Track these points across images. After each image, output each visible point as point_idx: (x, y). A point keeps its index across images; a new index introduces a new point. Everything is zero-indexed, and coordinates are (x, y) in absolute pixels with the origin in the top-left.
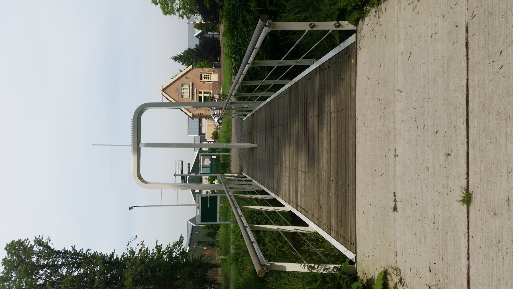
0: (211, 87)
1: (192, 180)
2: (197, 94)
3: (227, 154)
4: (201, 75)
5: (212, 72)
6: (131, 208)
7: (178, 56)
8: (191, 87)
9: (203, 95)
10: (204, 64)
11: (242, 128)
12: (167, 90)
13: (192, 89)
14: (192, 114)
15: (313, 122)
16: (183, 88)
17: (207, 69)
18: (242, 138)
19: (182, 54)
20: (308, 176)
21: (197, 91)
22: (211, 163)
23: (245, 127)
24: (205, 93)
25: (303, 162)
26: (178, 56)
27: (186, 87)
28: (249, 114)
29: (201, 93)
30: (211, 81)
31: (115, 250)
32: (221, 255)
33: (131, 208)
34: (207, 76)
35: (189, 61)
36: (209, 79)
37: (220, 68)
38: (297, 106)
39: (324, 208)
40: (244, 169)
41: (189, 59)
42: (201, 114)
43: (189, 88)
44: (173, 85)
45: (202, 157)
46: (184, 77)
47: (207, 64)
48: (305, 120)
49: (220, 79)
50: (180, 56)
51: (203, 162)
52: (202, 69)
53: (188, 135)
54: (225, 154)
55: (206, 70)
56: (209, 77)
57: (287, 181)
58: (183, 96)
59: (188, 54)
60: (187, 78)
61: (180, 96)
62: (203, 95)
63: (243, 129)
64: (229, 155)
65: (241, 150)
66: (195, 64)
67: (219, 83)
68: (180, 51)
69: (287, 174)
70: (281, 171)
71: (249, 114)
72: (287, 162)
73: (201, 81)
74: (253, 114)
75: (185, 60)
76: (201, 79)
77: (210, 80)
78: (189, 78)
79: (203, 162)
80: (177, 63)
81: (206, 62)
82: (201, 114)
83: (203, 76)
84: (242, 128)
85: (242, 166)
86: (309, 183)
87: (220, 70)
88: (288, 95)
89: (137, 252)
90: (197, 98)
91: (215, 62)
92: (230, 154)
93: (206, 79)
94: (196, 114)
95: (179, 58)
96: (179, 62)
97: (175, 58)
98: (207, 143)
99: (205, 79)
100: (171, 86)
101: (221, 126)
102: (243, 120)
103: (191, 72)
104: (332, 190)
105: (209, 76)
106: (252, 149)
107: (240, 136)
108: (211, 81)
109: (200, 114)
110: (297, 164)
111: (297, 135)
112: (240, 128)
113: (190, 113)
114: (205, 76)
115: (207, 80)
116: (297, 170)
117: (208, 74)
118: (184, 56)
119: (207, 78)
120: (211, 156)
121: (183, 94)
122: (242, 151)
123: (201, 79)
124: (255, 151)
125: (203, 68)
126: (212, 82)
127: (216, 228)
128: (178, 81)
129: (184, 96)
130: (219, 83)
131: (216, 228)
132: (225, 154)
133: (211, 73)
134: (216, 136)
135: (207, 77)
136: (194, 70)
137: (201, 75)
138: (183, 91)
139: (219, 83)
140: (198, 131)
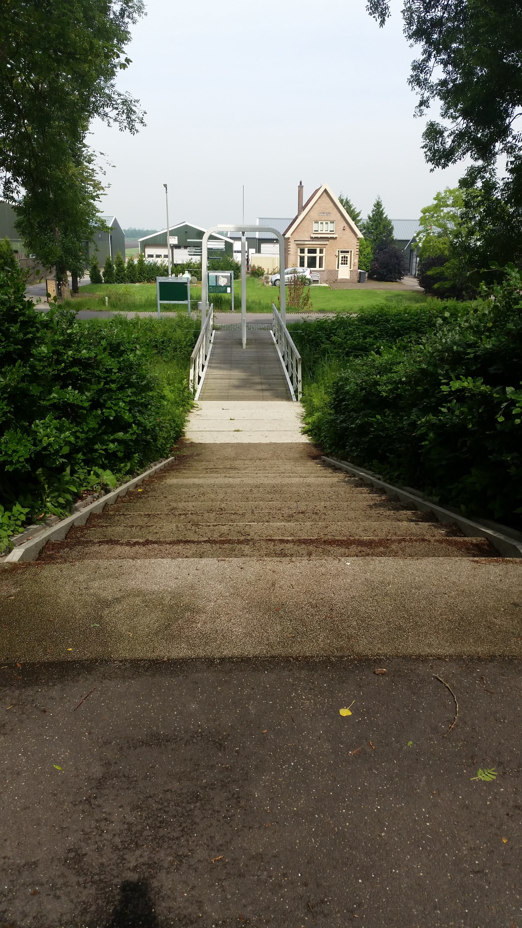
0: (330, 268)
1: (186, 232)
2: (319, 246)
3: (233, 306)
4: (348, 252)
5: (352, 269)
6: (165, 186)
7: (383, 210)
8: (329, 236)
9: (318, 255)
10: (368, 254)
11: (263, 329)
12: (325, 198)
13: (327, 238)
14: (289, 238)
15: (259, 387)
16: (329, 222)
17: (356, 261)
18: (252, 329)
19: (384, 216)
20: (228, 385)
21: (323, 246)
22: (221, 286)
23: (263, 334)
24: (321, 258)
25: (235, 382)
26: (383, 210)
27: (331, 227)
28: (275, 340)
29: (321, 251)
30: (338, 268)
31: (93, 134)
32: (109, 297)
33: (165, 186)
34: (347, 261)
35: (374, 227)
36: (342, 264)
37: (359, 282)
38: (271, 379)
39: (213, 391)
40: (219, 333)
41: (376, 229)
42: (289, 252)
43: (329, 232)
44: (334, 207)
45: (229, 274)
46: (346, 225)
47: (367, 258)
48: (261, 383)
49: (341, 282)
50: (382, 213)
51: (223, 277)
52: (358, 253)
53: (258, 219)
54: (233, 304)
55: (355, 260)
56: (344, 264)
57: (220, 373)
58: (317, 222)
59: (384, 227)
60: (344, 230)
61: (317, 218)
62: (318, 255)
63: (262, 332)
64: (231, 309)
65: (238, 328)
66: (369, 239)
67: (336, 280)
68: (389, 213)
69: (225, 373)
70: (226, 369)
71: (275, 340)
72: (233, 374)
73: (339, 251)
74: (273, 344)
75: (375, 221)
76: (342, 252)
77: (340, 265)
78: (344, 232)
79: (223, 277)
80: (372, 208)
81: (371, 256)
82: (289, 252)
83: (346, 256)
84: (263, 329)
85: (221, 329)
86: (224, 385)
87: (355, 282)
88: (280, 374)
89: (91, 166)
90: (313, 246)
91: (367, 274)
92: (233, 309)
93: (342, 260)
94: (289, 244)
95: (378, 212)
96: (373, 211)
97: (378, 205)
98: (246, 250)
99: (342, 257)
100: (332, 204)
101: (270, 284)
102: (271, 331)
103: (353, 236)
104: (223, 394)
105: (347, 264)
106: (241, 344)
107: (254, 327)
108: (338, 268)
109: (289, 247)
110: (234, 379)
111: (253, 379)
112: (263, 326)
113: (291, 235)
114: (347, 257)
115: (340, 262)
116: (230, 379)
117: (349, 262)
118: (381, 219)
119: (343, 262)
120: (230, 287)
121: (320, 222)
122: (237, 329)
123: (342, 252)
124: (239, 347)
125: (358, 256)
126: (337, 269)
127: (119, 276)
128: (339, 215)
129: (317, 224)
130: (336, 281)
131: (119, 276)
132: (233, 304)
133: (350, 268)
134: (256, 273)
135: (345, 261)
136: (355, 241)
137: (348, 252)
138: (324, 222)
139: (336, 280)
140: (268, 238)
